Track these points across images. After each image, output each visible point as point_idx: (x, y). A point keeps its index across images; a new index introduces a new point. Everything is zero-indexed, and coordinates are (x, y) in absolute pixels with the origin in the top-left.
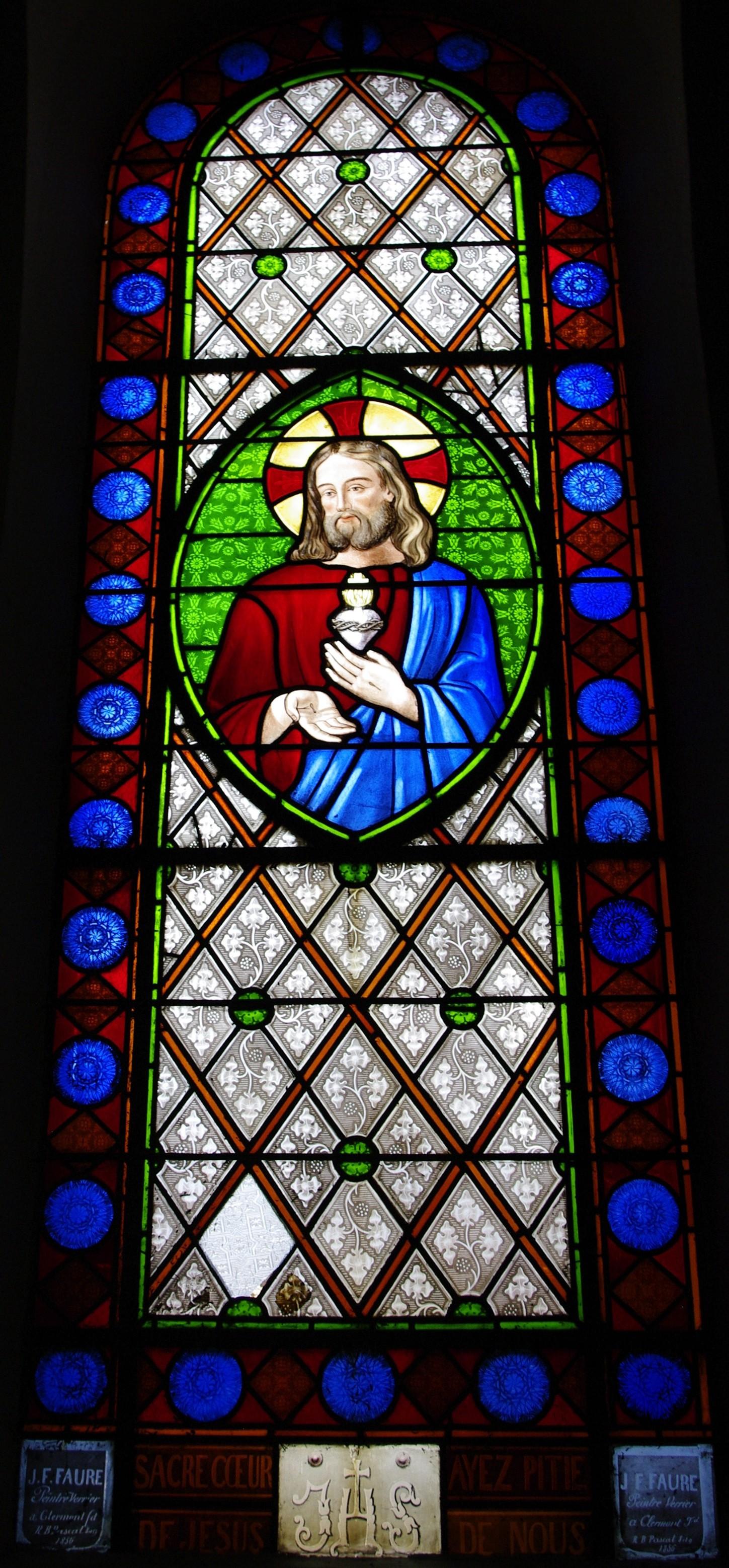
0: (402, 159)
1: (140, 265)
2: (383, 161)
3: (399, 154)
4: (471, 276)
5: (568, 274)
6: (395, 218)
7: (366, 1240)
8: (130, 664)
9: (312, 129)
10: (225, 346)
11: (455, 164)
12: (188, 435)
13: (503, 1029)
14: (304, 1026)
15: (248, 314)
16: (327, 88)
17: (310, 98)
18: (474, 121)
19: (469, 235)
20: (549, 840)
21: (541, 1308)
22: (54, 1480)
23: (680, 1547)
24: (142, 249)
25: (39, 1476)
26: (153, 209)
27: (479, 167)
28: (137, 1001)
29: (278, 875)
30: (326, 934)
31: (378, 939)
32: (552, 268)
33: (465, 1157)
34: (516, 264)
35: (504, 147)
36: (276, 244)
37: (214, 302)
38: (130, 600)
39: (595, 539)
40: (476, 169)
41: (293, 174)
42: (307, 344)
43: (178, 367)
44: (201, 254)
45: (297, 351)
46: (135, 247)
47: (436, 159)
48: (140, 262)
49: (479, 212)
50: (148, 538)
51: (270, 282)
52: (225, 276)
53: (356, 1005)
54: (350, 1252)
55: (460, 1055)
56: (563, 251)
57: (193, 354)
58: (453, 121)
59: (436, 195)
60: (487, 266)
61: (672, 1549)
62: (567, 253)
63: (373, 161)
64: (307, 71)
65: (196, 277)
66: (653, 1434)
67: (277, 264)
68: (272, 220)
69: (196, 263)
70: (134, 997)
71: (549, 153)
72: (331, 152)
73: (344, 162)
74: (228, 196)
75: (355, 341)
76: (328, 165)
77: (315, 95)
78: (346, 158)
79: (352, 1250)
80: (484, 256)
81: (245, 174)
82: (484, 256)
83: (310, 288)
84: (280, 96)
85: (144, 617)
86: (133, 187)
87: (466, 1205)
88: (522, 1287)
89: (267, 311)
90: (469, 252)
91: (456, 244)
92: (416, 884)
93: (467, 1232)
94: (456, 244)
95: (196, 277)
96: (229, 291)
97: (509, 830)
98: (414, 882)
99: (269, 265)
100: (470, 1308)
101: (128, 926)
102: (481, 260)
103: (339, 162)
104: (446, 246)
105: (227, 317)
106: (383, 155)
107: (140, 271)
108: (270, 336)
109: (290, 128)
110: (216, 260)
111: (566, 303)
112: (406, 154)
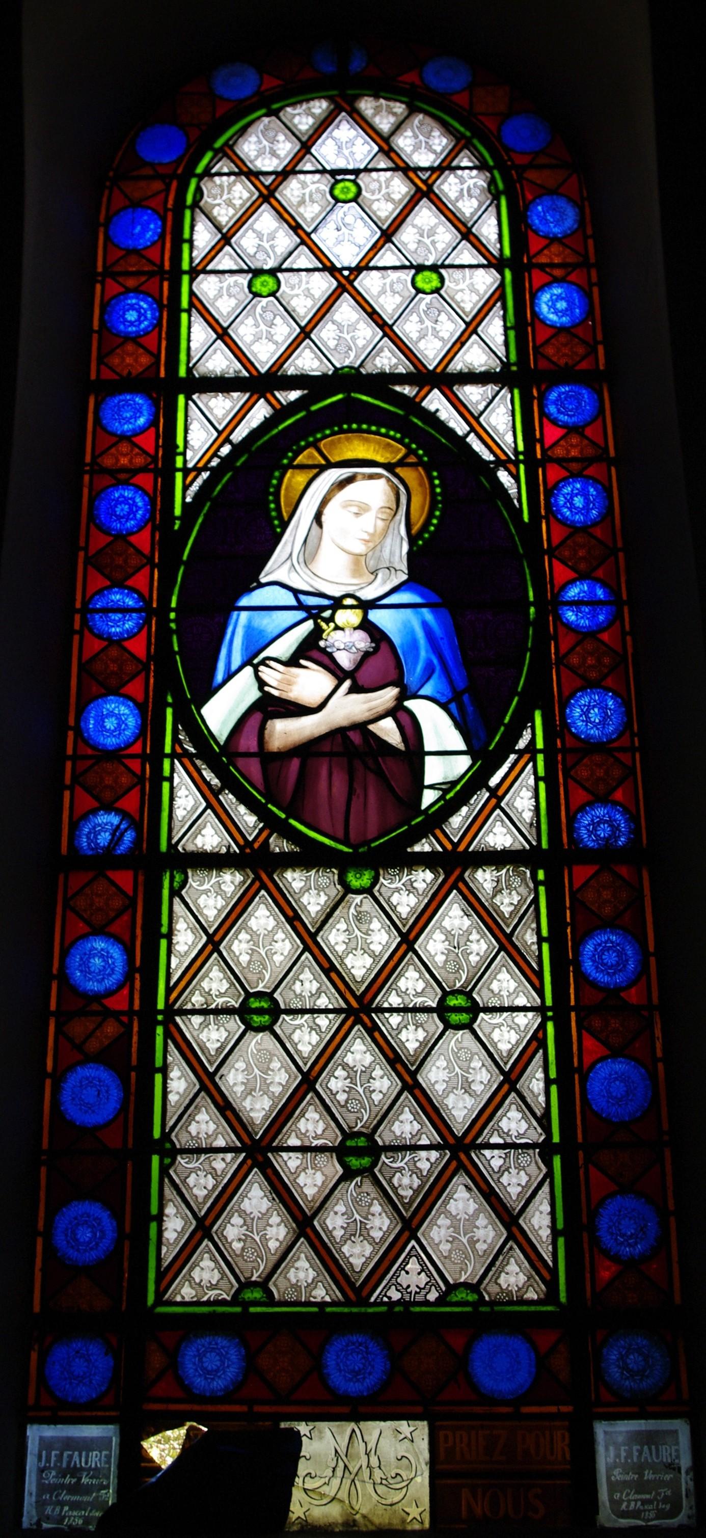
0: (392, 178)
1: (123, 477)
2: (374, 180)
3: (389, 174)
4: (458, 297)
5: (568, 490)
6: (387, 235)
7: (366, 1229)
8: (120, 913)
9: (306, 146)
10: (219, 362)
11: (442, 183)
12: (194, 265)
13: (497, 1030)
14: (306, 1136)
15: (244, 333)
16: (320, 107)
17: (303, 118)
18: (460, 144)
19: (457, 256)
20: (536, 849)
21: (532, 1295)
22: (62, 1463)
23: (661, 1515)
24: (124, 461)
25: (48, 1460)
26: (148, 232)
27: (465, 188)
28: (141, 1021)
29: (280, 1160)
30: (328, 1222)
31: (380, 1229)
32: (532, 252)
33: (460, 1150)
34: (502, 285)
35: (490, 169)
36: (270, 264)
37: (211, 321)
38: (130, 616)
39: (590, 661)
40: (462, 190)
41: (287, 192)
42: (300, 363)
43: (173, 385)
44: (194, 273)
45: (290, 369)
46: (118, 460)
47: (424, 178)
48: (123, 476)
49: (467, 234)
50: (152, 451)
51: (264, 301)
52: (219, 292)
53: (345, 281)
54: (350, 1239)
55: (457, 1053)
56: (564, 467)
57: (189, 370)
58: (440, 142)
59: (425, 215)
60: (475, 285)
61: (652, 1515)
62: (567, 470)
63: (363, 180)
64: (300, 93)
65: (192, 294)
66: (635, 1409)
67: (270, 281)
68: (265, 238)
69: (192, 281)
70: (148, 751)
71: (531, 175)
72: (323, 171)
73: (337, 182)
74: (225, 215)
75: (350, 360)
76: (322, 184)
77: (309, 113)
78: (339, 177)
79: (352, 1238)
80: (471, 278)
81: (241, 192)
82: (471, 278)
83: (304, 308)
84: (275, 113)
85: (150, 525)
86: (125, 208)
87: (461, 1200)
88: (514, 1276)
89: (265, 147)
90: (457, 274)
91: (443, 266)
92: (421, 1171)
93: (461, 1230)
94: (443, 266)
95: (192, 294)
96: (223, 308)
97: (498, 836)
98: (418, 1168)
99: (264, 284)
100: (467, 1294)
101: (129, 951)
102: (468, 282)
103: (333, 181)
104: (434, 268)
105: (223, 334)
106: (374, 175)
107: (126, 484)
108: (264, 356)
109: (286, 148)
110: (213, 278)
111: (564, 522)
112: (396, 174)
